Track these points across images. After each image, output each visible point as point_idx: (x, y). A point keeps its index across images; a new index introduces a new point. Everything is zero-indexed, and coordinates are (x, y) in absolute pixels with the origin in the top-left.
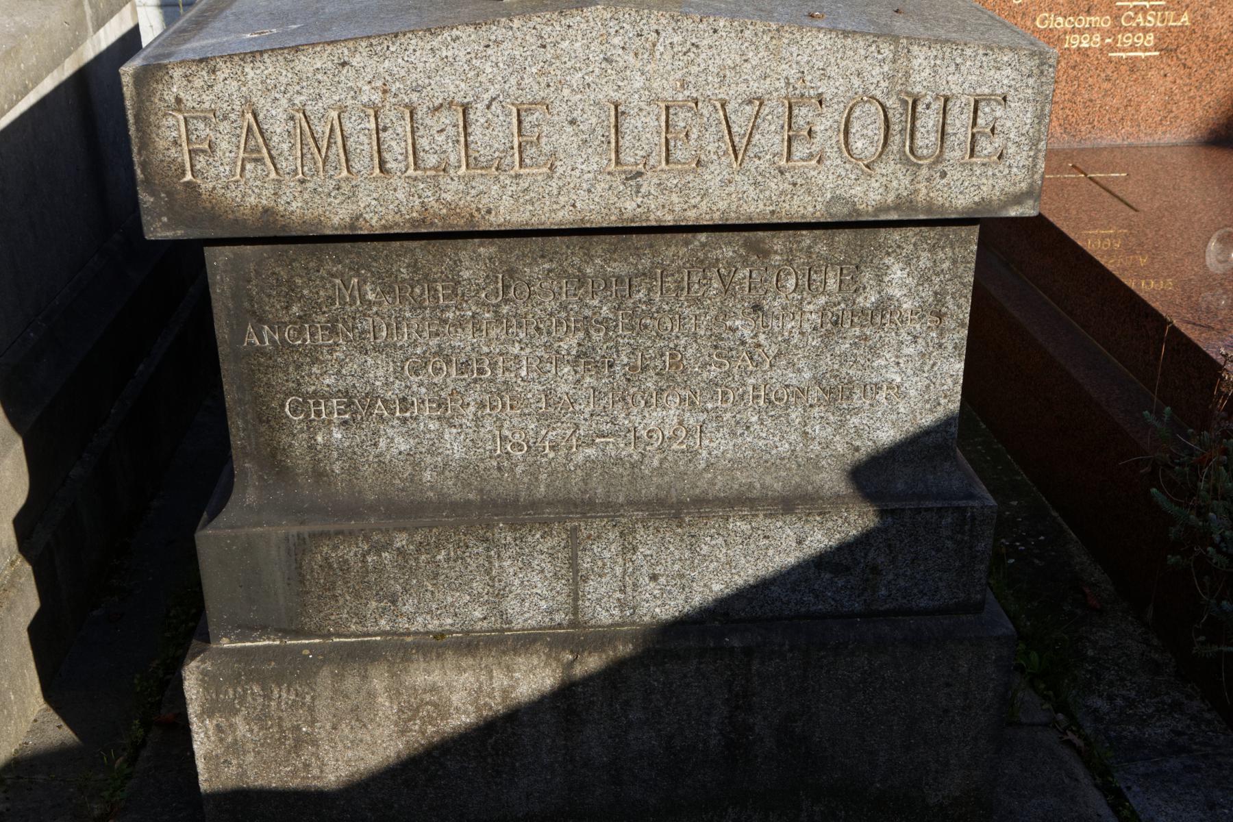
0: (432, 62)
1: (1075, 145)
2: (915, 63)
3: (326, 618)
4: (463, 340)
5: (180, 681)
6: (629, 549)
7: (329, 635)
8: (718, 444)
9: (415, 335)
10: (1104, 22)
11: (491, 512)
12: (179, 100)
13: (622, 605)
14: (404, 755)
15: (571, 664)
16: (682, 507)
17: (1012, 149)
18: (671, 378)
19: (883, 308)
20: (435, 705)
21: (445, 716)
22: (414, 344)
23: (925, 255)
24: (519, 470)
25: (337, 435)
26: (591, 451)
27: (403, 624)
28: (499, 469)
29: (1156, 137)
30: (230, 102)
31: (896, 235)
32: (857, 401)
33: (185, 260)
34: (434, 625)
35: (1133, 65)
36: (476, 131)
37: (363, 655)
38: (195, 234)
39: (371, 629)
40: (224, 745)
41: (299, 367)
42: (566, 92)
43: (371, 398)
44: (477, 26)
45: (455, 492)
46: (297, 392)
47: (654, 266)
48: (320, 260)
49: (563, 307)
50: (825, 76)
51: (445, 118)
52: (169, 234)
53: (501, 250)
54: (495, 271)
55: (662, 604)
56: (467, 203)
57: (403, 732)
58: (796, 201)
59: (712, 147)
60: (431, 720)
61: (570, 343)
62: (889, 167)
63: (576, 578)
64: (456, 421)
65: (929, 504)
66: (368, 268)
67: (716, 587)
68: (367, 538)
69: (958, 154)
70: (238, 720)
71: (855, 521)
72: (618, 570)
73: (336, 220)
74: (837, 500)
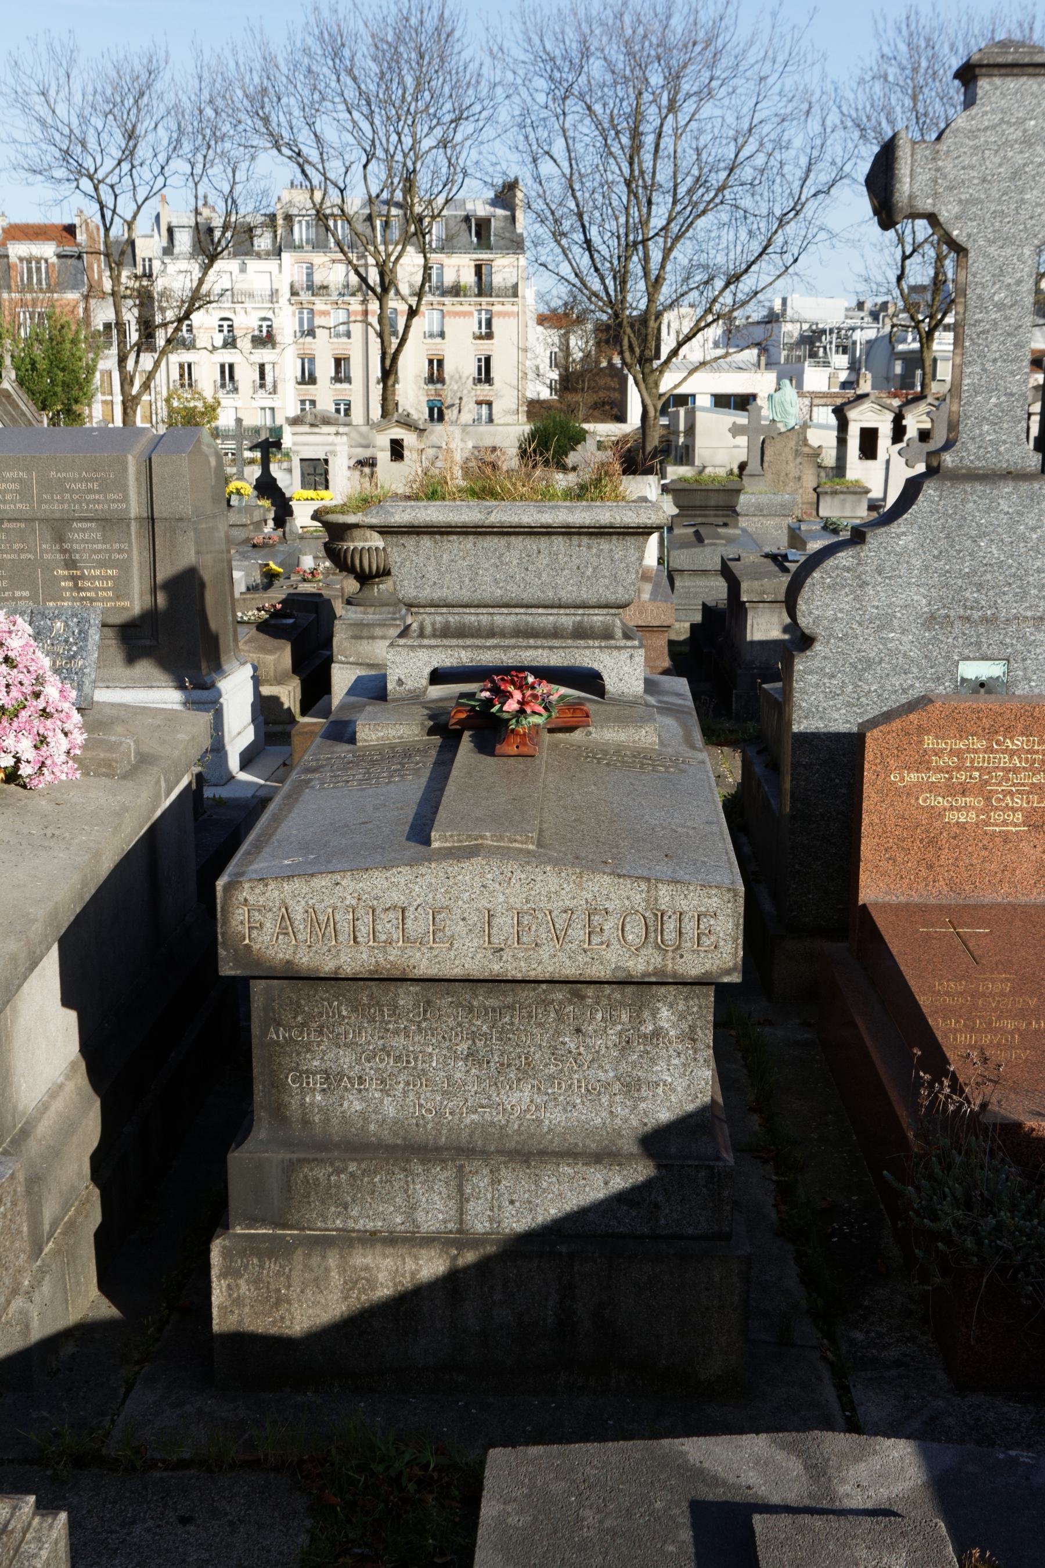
0: (386, 884)
1: (961, 902)
2: (661, 893)
3: (303, 1216)
4: (398, 1042)
5: (208, 1251)
6: (495, 1182)
7: (303, 1229)
8: (555, 1117)
9: (369, 1038)
10: (978, 802)
11: (411, 1151)
12: (246, 900)
13: (491, 1220)
14: (346, 1314)
15: (455, 1258)
16: (530, 1154)
17: (722, 943)
18: (525, 1072)
19: (657, 1033)
20: (368, 1280)
21: (373, 1288)
22: (369, 1043)
23: (681, 1002)
24: (429, 1126)
25: (319, 1098)
26: (475, 1117)
27: (351, 1224)
28: (417, 1125)
29: (1032, 897)
30: (274, 902)
31: (663, 990)
32: (644, 1093)
33: (240, 987)
34: (370, 1226)
35: (1006, 838)
36: (409, 922)
37: (324, 1243)
38: (247, 973)
39: (330, 1226)
40: (234, 1300)
41: (298, 1054)
42: (460, 903)
43: (341, 1075)
44: (411, 866)
45: (386, 1135)
46: (296, 1069)
47: (515, 1002)
48: (316, 990)
49: (460, 1025)
50: (608, 899)
51: (391, 915)
52: (232, 973)
53: (423, 988)
54: (419, 1001)
55: (517, 1221)
56: (402, 962)
57: (346, 1298)
58: (594, 968)
59: (544, 936)
60: (364, 1291)
61: (463, 1047)
62: (649, 950)
63: (462, 1200)
64: (392, 1093)
65: (690, 1162)
66: (344, 996)
67: (553, 1211)
68: (332, 1164)
69: (689, 944)
70: (242, 1282)
71: (640, 1172)
72: (489, 1196)
73: (327, 969)
74: (631, 1156)
